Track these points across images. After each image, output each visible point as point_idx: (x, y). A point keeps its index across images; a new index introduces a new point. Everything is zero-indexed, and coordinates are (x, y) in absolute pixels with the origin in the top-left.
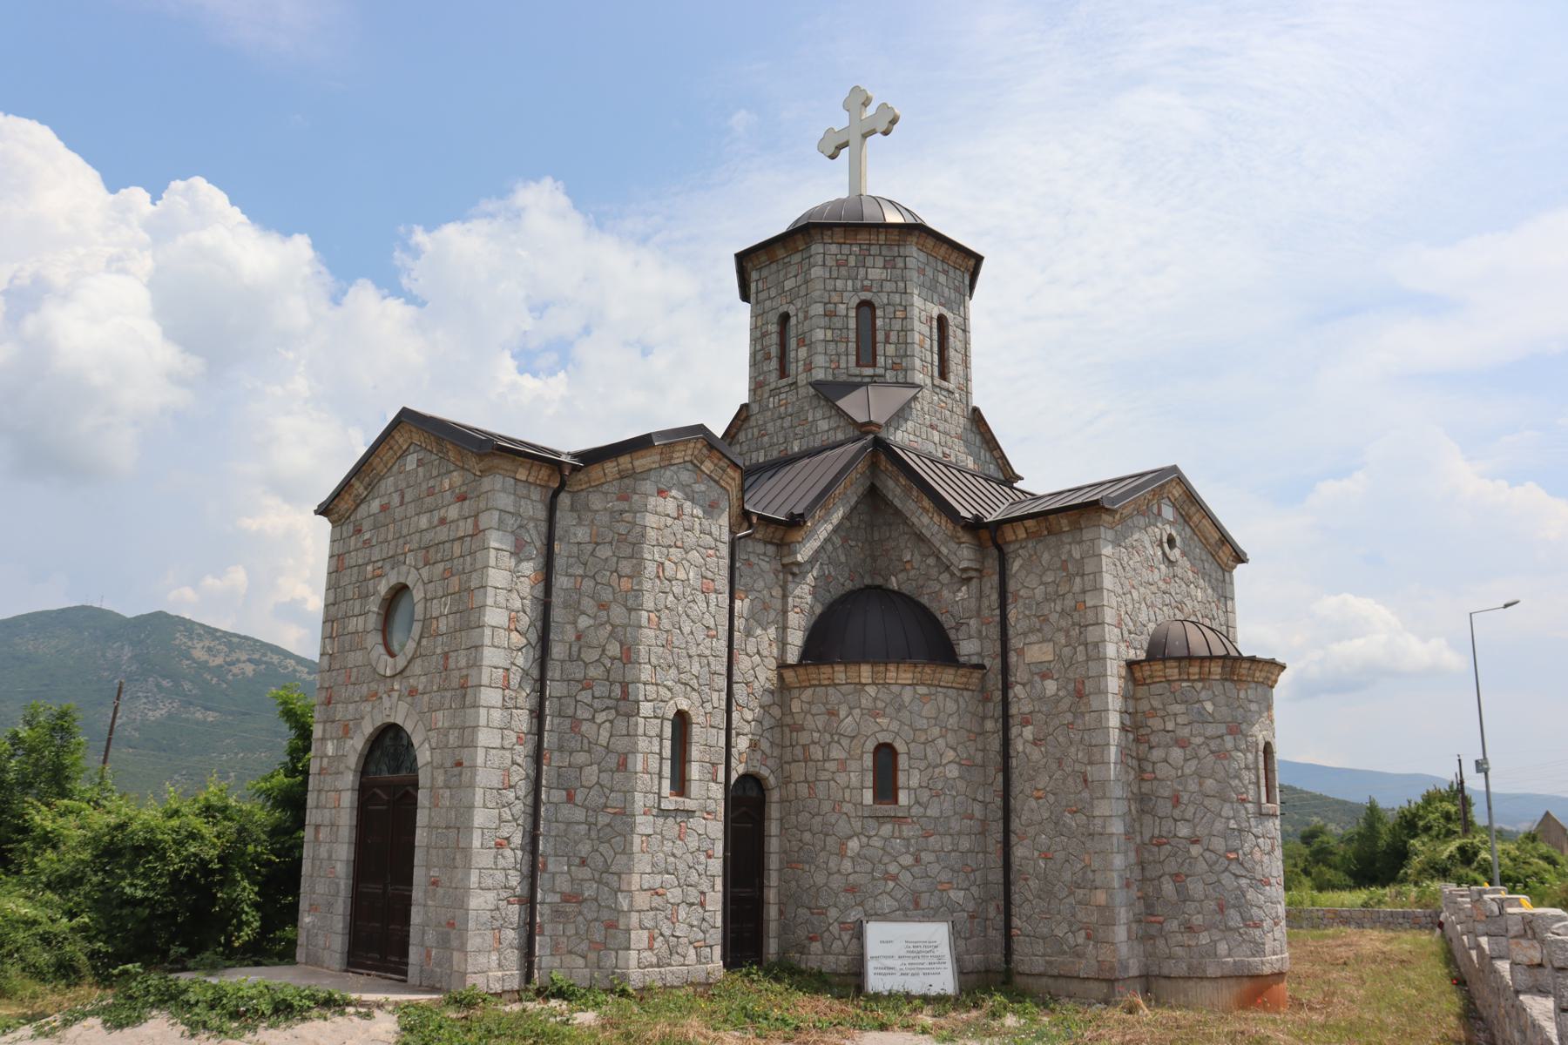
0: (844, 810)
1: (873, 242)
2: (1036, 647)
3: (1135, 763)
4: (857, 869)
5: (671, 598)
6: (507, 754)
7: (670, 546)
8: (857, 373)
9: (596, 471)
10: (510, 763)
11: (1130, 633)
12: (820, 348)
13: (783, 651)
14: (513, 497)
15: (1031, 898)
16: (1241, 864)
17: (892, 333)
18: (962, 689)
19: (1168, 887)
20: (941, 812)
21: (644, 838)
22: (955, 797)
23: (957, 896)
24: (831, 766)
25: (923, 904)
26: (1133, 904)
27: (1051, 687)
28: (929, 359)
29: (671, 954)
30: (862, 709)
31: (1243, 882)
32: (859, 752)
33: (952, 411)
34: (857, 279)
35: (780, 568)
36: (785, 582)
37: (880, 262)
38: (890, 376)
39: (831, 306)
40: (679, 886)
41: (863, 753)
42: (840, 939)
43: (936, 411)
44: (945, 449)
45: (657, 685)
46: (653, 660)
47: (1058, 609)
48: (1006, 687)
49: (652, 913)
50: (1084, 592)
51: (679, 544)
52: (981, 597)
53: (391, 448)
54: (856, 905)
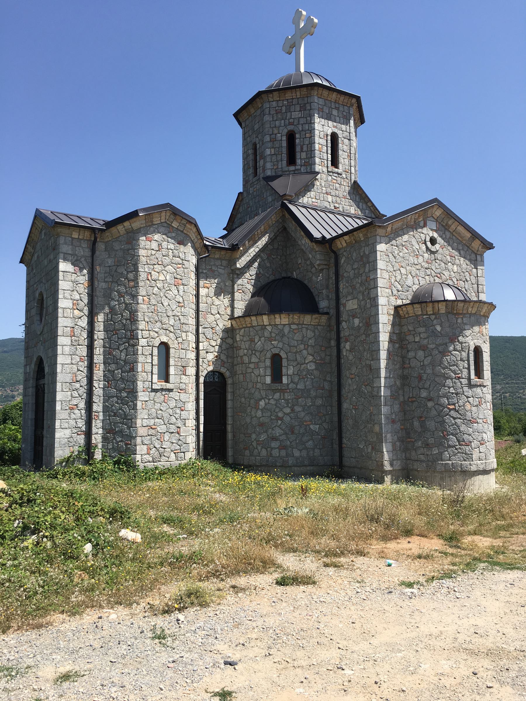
0: (258, 387)
1: (294, 97)
2: (351, 301)
3: (400, 359)
4: (264, 414)
5: (156, 289)
6: (75, 366)
7: (155, 265)
8: (287, 169)
9: (114, 230)
10: (76, 370)
11: (398, 291)
12: (268, 159)
13: (233, 311)
14: (71, 246)
15: (350, 429)
16: (457, 411)
17: (304, 146)
18: (317, 325)
19: (416, 424)
20: (305, 386)
21: (143, 402)
22: (312, 379)
23: (315, 427)
24: (252, 366)
25: (296, 431)
26: (398, 432)
27: (357, 321)
28: (325, 158)
29: (161, 456)
30: (265, 337)
31: (458, 421)
32: (264, 358)
33: (340, 184)
34: (286, 119)
35: (230, 271)
36: (233, 278)
37: (298, 108)
38: (303, 169)
39: (273, 136)
40: (164, 424)
41: (265, 359)
42: (257, 448)
43: (330, 185)
44: (336, 205)
45: (149, 330)
46: (146, 319)
47: (359, 281)
48: (338, 323)
49: (149, 437)
50: (370, 271)
51: (160, 263)
52: (329, 278)
53: (36, 229)
54: (264, 432)
